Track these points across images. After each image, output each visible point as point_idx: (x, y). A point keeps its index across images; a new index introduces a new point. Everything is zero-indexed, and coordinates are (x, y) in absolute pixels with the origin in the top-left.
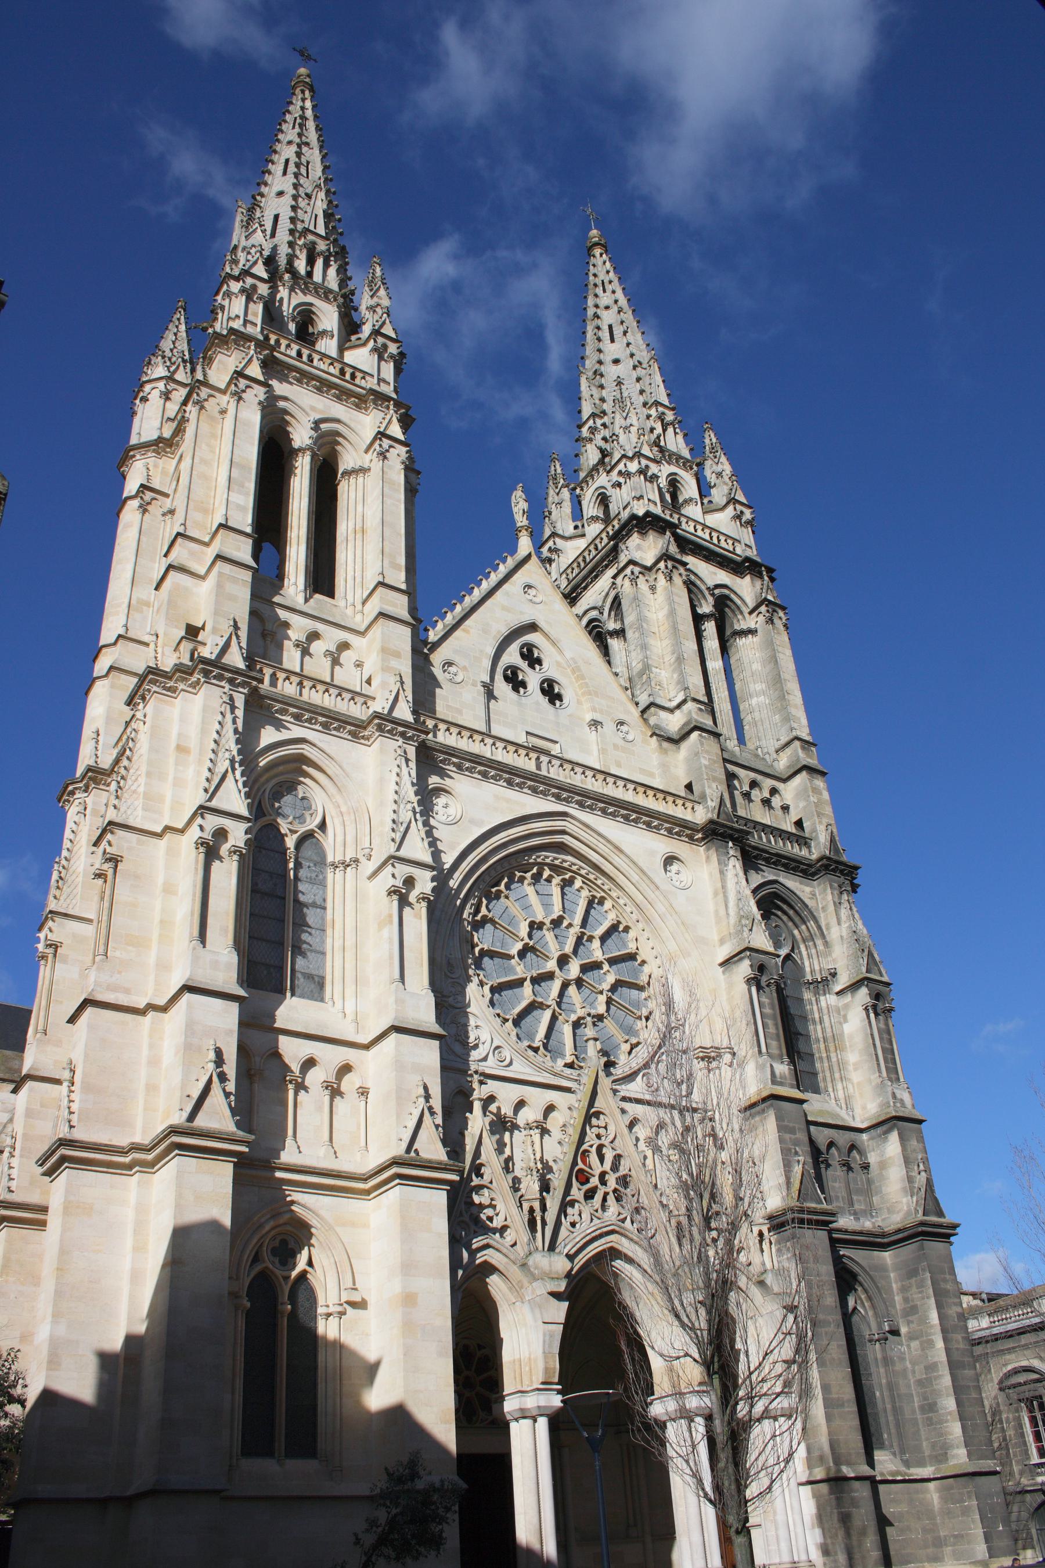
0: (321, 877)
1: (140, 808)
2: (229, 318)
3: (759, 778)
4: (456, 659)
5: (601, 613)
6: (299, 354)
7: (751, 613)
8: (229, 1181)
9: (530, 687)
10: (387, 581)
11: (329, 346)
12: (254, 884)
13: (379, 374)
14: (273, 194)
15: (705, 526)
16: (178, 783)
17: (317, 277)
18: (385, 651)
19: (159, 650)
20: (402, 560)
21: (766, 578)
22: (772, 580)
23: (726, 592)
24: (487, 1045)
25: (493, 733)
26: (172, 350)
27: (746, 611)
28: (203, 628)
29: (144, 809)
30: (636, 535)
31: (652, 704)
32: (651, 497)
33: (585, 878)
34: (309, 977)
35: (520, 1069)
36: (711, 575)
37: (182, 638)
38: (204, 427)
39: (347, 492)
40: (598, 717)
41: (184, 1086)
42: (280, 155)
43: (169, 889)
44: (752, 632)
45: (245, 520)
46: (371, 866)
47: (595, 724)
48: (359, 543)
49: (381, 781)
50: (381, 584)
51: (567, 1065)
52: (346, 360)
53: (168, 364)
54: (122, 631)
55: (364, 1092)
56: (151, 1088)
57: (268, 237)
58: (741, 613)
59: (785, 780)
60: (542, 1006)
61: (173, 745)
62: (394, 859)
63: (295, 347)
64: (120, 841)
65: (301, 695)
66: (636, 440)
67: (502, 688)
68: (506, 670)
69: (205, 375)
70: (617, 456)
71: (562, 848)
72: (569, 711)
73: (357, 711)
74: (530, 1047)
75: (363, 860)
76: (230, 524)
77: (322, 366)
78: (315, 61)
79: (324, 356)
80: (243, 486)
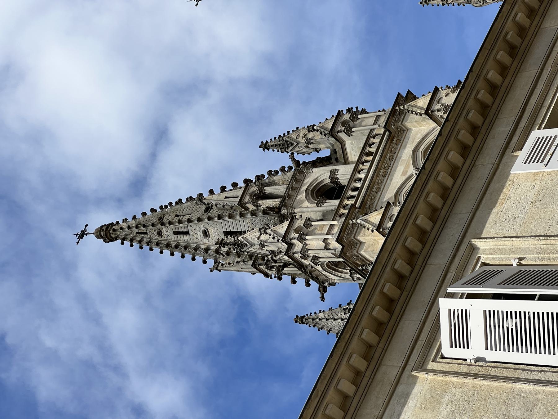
14: (206, 241)
15: (360, 161)
32: (325, 230)
42: (171, 240)
52: (356, 159)
66: (268, 236)
78: (86, 226)
79: (353, 178)
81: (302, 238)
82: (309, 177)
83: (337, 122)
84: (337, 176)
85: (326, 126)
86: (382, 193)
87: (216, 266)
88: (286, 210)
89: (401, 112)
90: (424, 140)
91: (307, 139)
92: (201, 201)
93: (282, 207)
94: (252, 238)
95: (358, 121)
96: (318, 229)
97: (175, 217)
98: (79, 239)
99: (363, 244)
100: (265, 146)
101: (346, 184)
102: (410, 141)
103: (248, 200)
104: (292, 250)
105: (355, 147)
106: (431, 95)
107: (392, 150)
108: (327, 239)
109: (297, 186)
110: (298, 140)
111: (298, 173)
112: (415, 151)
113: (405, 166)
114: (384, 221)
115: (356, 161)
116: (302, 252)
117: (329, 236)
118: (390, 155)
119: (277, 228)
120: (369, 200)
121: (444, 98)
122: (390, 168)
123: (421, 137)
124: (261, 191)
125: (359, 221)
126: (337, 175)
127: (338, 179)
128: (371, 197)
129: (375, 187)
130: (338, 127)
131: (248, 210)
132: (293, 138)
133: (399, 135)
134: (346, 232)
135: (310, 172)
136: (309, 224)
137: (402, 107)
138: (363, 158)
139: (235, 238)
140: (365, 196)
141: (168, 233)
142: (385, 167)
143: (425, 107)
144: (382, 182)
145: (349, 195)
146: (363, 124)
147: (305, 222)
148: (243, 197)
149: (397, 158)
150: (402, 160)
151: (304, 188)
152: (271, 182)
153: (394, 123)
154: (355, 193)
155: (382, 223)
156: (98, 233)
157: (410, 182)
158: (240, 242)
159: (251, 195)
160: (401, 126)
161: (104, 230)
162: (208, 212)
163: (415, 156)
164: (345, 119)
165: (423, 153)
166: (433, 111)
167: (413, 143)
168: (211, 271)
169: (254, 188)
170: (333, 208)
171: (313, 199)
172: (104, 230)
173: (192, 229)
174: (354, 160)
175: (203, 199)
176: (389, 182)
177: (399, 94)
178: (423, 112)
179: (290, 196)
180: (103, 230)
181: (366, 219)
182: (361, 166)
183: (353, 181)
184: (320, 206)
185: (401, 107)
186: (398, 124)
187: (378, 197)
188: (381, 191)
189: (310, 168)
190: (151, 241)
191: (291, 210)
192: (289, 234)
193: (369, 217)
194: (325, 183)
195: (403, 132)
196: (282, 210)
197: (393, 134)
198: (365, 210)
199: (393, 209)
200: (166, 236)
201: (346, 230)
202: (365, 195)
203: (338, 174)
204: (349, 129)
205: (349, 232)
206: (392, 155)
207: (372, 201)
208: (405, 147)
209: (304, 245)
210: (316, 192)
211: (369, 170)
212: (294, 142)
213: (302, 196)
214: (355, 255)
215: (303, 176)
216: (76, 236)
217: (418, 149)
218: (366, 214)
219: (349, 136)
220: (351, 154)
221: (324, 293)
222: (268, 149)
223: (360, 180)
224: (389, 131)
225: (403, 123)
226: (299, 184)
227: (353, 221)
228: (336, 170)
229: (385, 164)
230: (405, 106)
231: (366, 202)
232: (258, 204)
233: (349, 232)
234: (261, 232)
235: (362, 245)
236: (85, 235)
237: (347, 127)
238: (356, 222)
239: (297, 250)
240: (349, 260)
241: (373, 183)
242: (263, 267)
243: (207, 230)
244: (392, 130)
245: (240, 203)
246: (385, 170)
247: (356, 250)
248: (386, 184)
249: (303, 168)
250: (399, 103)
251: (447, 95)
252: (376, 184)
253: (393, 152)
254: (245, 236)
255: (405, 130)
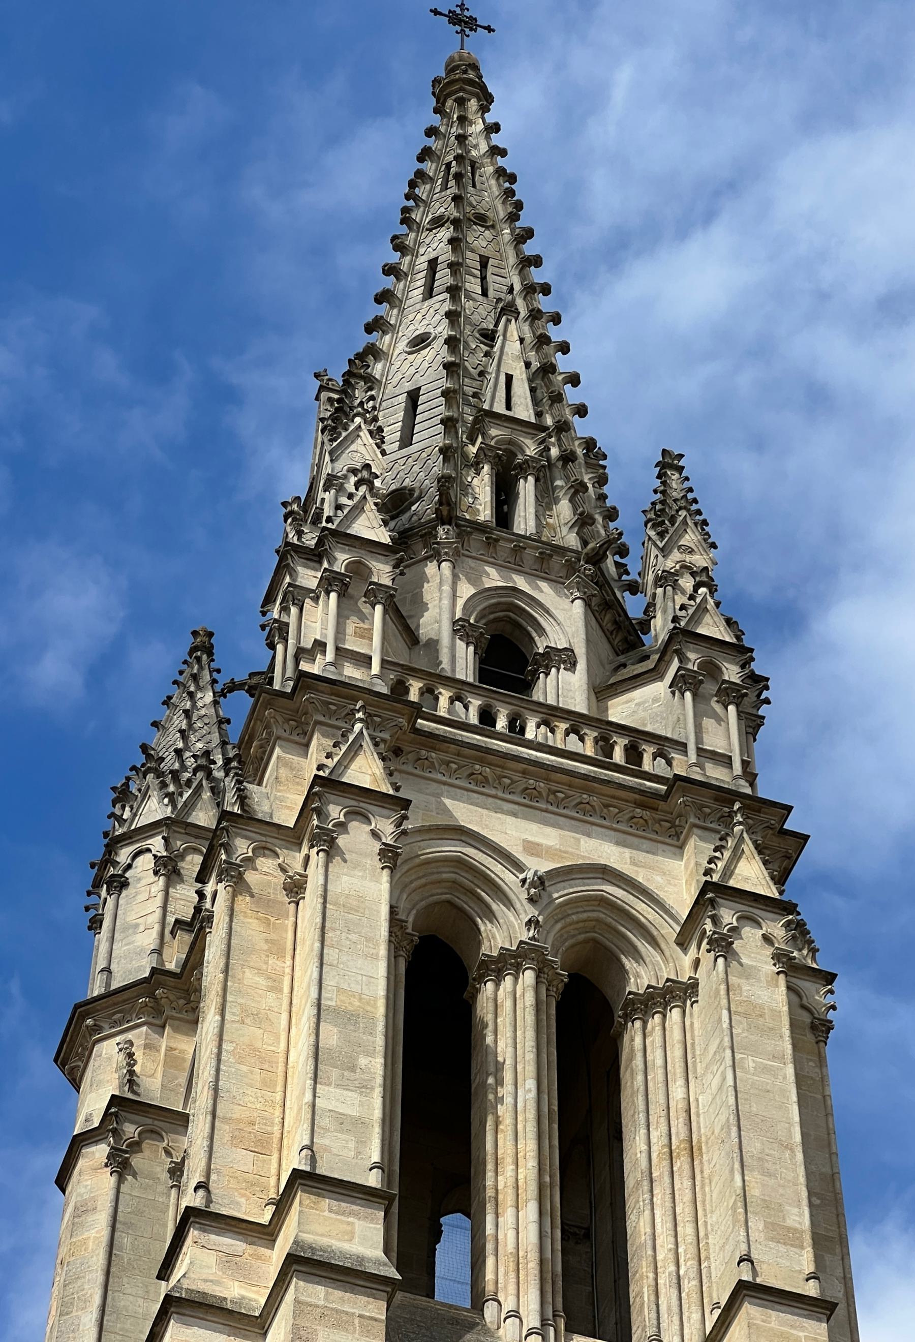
6: (487, 717)
14: (402, 345)
32: (351, 644)
52: (612, 719)
63: (475, 703)
78: (436, 12)
82: (558, 593)
83: (713, 648)
84: (553, 670)
86: (469, 793)
87: (330, 386)
88: (446, 538)
89: (727, 820)
90: (641, 894)
91: (676, 574)
92: (503, 312)
93: (457, 526)
94: (355, 454)
96: (362, 625)
97: (480, 255)
98: (447, 13)
99: (302, 753)
101: (535, 698)
102: (642, 856)
103: (493, 435)
104: (303, 560)
105: (645, 710)
106: (773, 896)
107: (611, 809)
108: (324, 652)
110: (676, 550)
111: (566, 561)
112: (605, 873)
113: (556, 850)
114: (346, 795)
115: (608, 717)
116: (291, 589)
118: (594, 804)
119: (370, 514)
120: (443, 756)
121: (368, 828)
122: (550, 808)
123: (651, 886)
124: (521, 469)
125: (358, 726)
126: (558, 670)
127: (547, 674)
128: (505, 777)
129: (488, 769)
130: (696, 651)
131: (471, 440)
132: (681, 537)
133: (662, 823)
134: (334, 699)
135: (572, 594)
136: (375, 597)
137: (739, 818)
138: (588, 729)
139: (360, 409)
140: (454, 742)
141: (434, 246)
142: (555, 792)
145: (469, 699)
146: (708, 723)
147: (381, 585)
148: (504, 421)
149: (588, 826)
150: (579, 840)
151: (521, 583)
152: (553, 494)
153: (692, 802)
154: (618, 756)
155: (340, 791)
156: (460, 61)
157: (500, 866)
158: (346, 423)
159: (511, 442)
160: (687, 827)
161: (465, 76)
162: (481, 338)
163: (588, 873)
164: (724, 669)
165: (597, 896)
166: (712, 902)
167: (636, 865)
168: (317, 376)
169: (532, 449)
171: (484, 609)
172: (465, 76)
173: (437, 306)
174: (610, 712)
175: (510, 317)
176: (505, 808)
177: (789, 809)
179: (495, 547)
180: (465, 72)
181: (361, 746)
182: (591, 735)
183: (545, 716)
184: (454, 630)
185: (739, 815)
186: (692, 816)
187: (457, 782)
188: (476, 788)
189: (585, 593)
190: (421, 204)
191: (446, 553)
192: (347, 548)
193: (368, 753)
194: (537, 638)
195: (674, 833)
196: (447, 527)
198: (413, 749)
199: (388, 818)
200: (427, 241)
201: (338, 697)
202: (460, 743)
203: (562, 670)
204: (690, 684)
205: (333, 707)
206: (597, 808)
207: (444, 766)
209: (313, 591)
210: (510, 618)
211: (545, 749)
212: (666, 539)
213: (494, 578)
214: (270, 734)
215: (561, 577)
216: (457, 6)
217: (610, 880)
218: (760, 849)
219: (670, 687)
220: (627, 702)
221: (246, 688)
222: (659, 477)
224: (669, 792)
225: (695, 830)
226: (535, 567)
227: (358, 711)
229: (509, 778)
230: (741, 827)
231: (437, 746)
232: (481, 465)
233: (331, 706)
234: (361, 471)
235: (677, 851)
236: (458, 28)
237: (695, 677)
238: (357, 720)
239: (300, 575)
240: (257, 720)
241: (500, 763)
243: (429, 345)
244: (674, 801)
245: (481, 415)
246: (544, 794)
247: (285, 735)
248: (499, 802)
249: (584, 574)
250: (760, 812)
251: (767, 939)
252: (498, 771)
253: (605, 811)
254: (364, 434)
255: (678, 839)
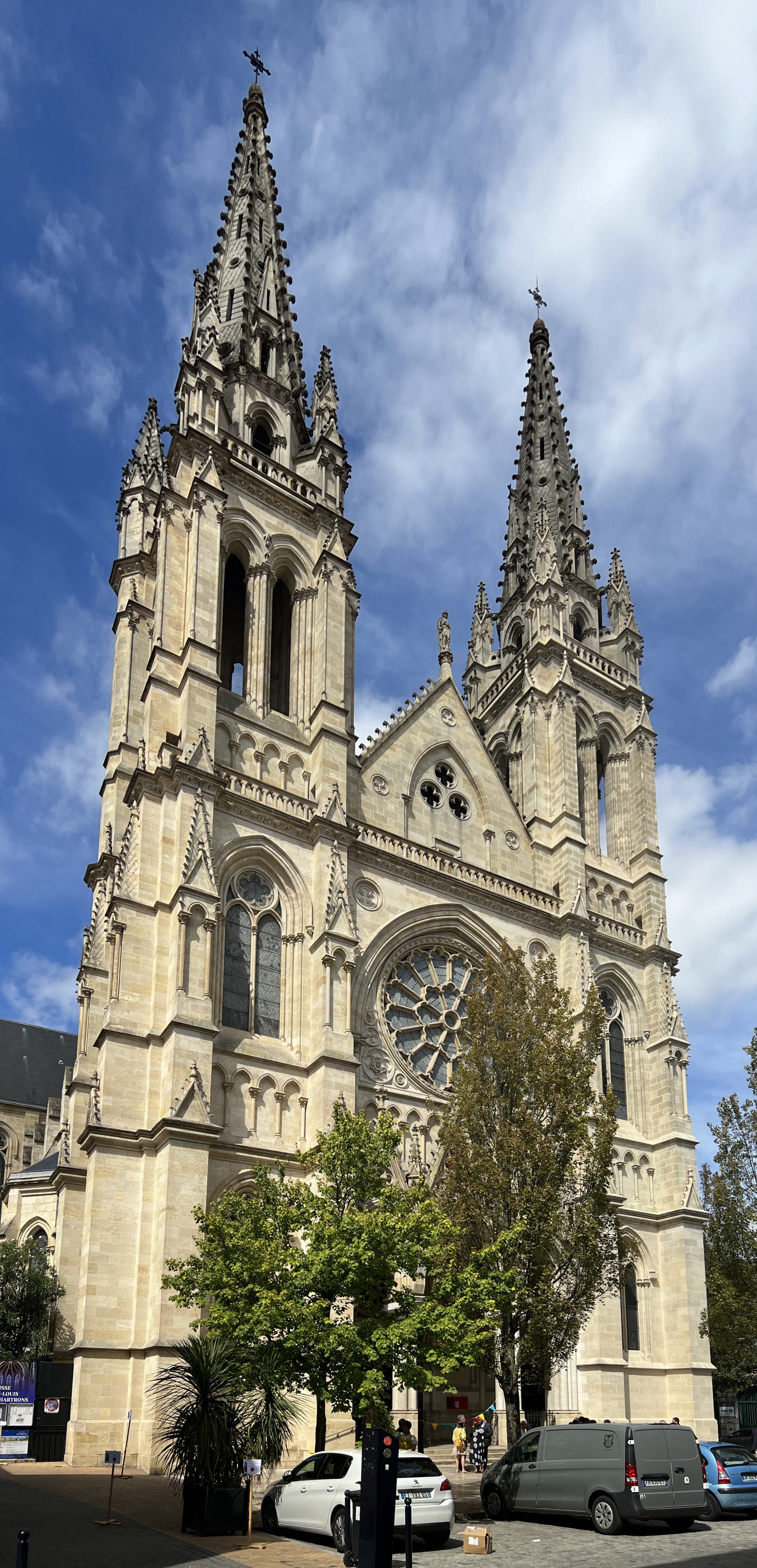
0: (277, 947)
1: (137, 887)
2: (189, 417)
3: (612, 883)
4: (386, 775)
5: (506, 738)
6: (255, 463)
7: (626, 740)
8: (207, 1156)
9: (441, 802)
10: (329, 700)
11: (282, 455)
12: (227, 950)
13: (326, 489)
16: (165, 868)
17: (271, 372)
18: (325, 763)
19: (146, 756)
20: (341, 681)
21: (644, 707)
22: (649, 708)
23: (609, 720)
24: (392, 1073)
25: (410, 839)
26: (146, 456)
27: (623, 737)
28: (180, 737)
29: (140, 888)
30: (539, 665)
31: (535, 819)
32: (208, 418)
33: (471, 958)
34: (268, 1021)
35: (413, 1091)
36: (599, 704)
37: (163, 744)
38: (173, 539)
39: (301, 612)
40: (492, 828)
41: (173, 1092)
42: (234, 211)
43: (162, 951)
44: (624, 757)
45: (210, 636)
46: (310, 942)
47: (489, 834)
48: (308, 664)
49: (320, 874)
50: (323, 703)
51: (446, 1089)
52: (298, 473)
53: (144, 473)
54: (123, 740)
55: (304, 1103)
56: (154, 1094)
57: (223, 319)
58: (619, 739)
59: (633, 886)
60: (433, 1049)
61: (161, 838)
62: (328, 936)
64: (125, 914)
65: (261, 800)
67: (419, 800)
68: (423, 785)
69: (169, 482)
70: (531, 584)
71: (456, 933)
72: (470, 822)
73: (302, 815)
74: (422, 1076)
75: (307, 936)
76: (197, 640)
77: (278, 479)
79: (278, 467)
80: (207, 603)
81: (550, 601)
85: (333, 434)
95: (333, 476)
100: (325, 353)
102: (305, 536)
109: (272, 393)
112: (291, 539)
117: (200, 422)
121: (213, 504)
125: (210, 457)
134: (201, 442)
143: (332, 552)
144: (260, 497)
146: (330, 482)
151: (269, 402)
170: (241, 435)
178: (327, 549)
182: (290, 479)
197: (312, 515)
208: (297, 528)
222: (613, 558)
223: (591, 660)
228: (285, 447)
236: (255, 68)
242: (514, 550)
